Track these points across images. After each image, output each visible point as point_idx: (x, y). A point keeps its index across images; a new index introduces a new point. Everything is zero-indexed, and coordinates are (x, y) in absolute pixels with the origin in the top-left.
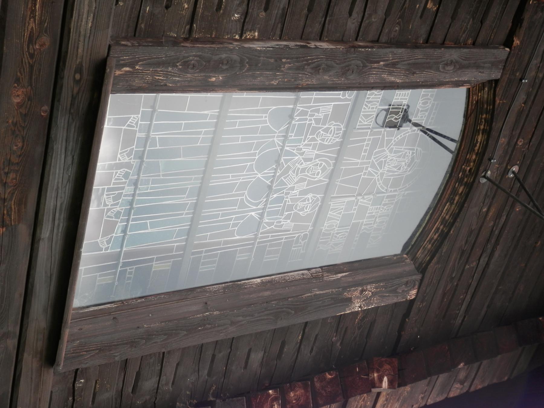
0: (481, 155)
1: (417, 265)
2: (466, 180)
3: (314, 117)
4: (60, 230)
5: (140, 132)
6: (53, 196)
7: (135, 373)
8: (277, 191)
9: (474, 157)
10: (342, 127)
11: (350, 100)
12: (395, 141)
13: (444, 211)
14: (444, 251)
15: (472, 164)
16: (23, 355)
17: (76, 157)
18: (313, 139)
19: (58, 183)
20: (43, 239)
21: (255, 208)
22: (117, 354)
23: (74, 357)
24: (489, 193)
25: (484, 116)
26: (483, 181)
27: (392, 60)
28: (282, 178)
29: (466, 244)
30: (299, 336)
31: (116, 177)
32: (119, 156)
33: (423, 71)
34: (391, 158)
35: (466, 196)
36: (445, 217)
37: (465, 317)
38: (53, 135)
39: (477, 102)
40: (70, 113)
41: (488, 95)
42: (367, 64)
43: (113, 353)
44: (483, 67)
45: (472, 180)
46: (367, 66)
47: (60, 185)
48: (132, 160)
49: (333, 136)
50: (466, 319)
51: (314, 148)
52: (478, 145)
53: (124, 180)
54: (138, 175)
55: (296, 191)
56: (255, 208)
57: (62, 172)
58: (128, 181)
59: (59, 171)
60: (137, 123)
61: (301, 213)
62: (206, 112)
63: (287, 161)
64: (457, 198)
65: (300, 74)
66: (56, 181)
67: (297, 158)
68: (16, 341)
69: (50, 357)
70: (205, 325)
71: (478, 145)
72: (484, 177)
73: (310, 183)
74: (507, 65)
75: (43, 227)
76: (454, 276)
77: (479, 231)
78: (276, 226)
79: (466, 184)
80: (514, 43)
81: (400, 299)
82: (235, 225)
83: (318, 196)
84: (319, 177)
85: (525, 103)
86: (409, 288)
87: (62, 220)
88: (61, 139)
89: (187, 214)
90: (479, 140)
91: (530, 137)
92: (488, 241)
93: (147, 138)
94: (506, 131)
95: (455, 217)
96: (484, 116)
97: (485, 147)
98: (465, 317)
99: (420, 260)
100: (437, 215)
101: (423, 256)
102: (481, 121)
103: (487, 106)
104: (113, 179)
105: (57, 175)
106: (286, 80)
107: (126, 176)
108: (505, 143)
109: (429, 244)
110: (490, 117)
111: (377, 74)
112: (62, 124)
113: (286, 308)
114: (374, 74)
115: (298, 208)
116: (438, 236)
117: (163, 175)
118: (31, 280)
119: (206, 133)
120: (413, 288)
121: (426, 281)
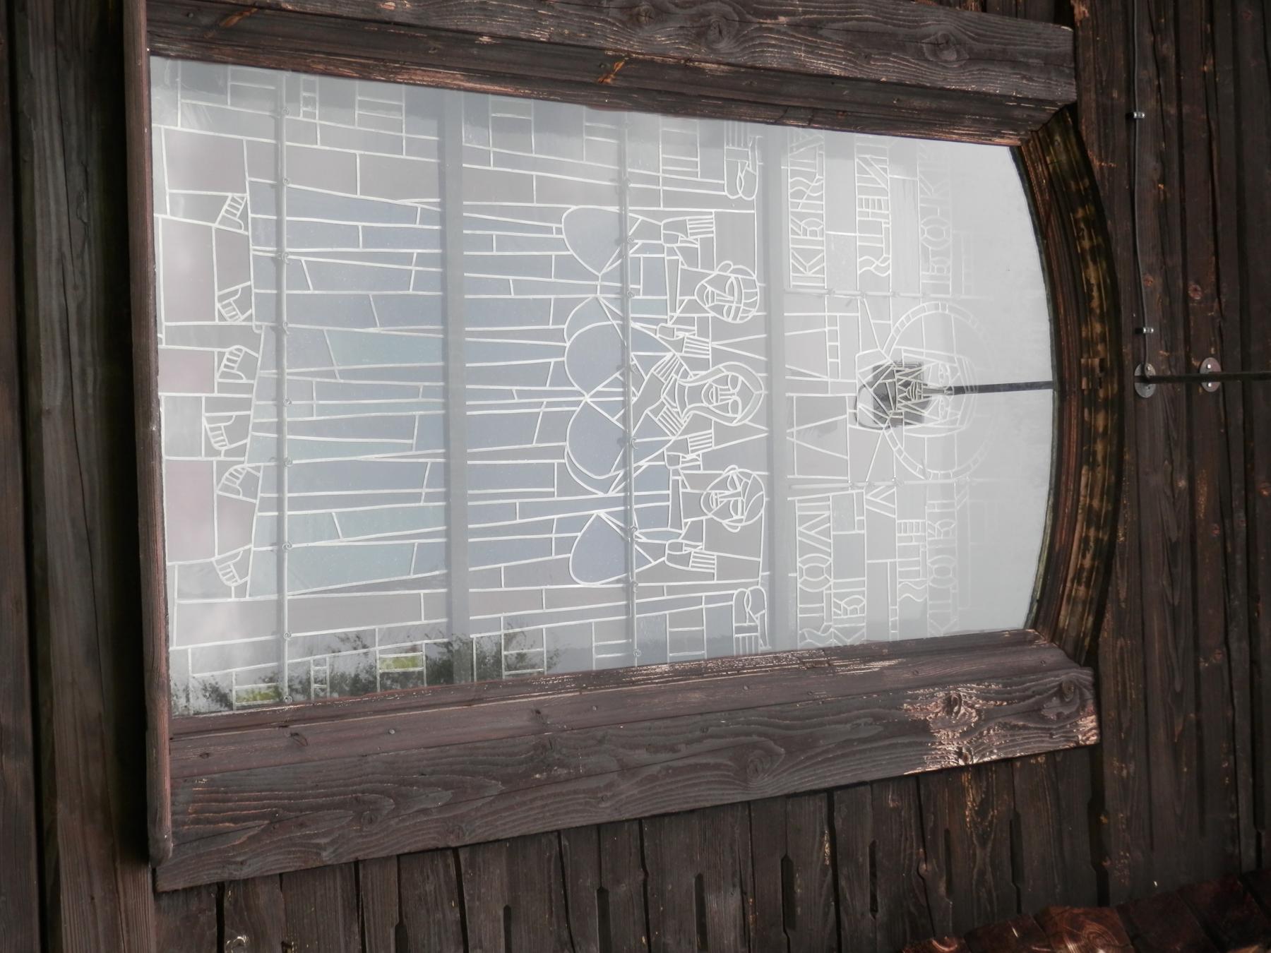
0: (1112, 314)
1: (1069, 648)
2: (1101, 393)
3: (679, 244)
4: (90, 390)
5: (257, 243)
6: (54, 281)
7: (392, 932)
8: (648, 449)
9: (1098, 328)
10: (755, 277)
11: (749, 205)
12: (897, 330)
13: (1083, 491)
14: (1123, 595)
15: (1100, 347)
16: (54, 813)
17: (94, 170)
18: (693, 306)
19: (60, 240)
20: (49, 412)
21: (601, 495)
22: (323, 841)
23: (201, 838)
24: (1174, 435)
25: (1080, 213)
26: (1148, 391)
27: (805, 13)
28: (647, 411)
29: (1172, 584)
30: (822, 845)
31: (222, 369)
32: (218, 305)
33: (889, 54)
34: (905, 379)
35: (1119, 435)
36: (1091, 506)
37: (1259, 837)
38: (24, 107)
39: (1050, 181)
40: (56, 42)
41: (1067, 151)
42: (749, 17)
43: (310, 837)
44: (1027, 66)
45: (1116, 386)
46: (750, 22)
47: (66, 249)
48: (254, 323)
49: (740, 301)
50: (1264, 844)
51: (703, 332)
52: (1095, 293)
53: (244, 381)
54: (279, 366)
55: (693, 456)
56: (601, 495)
57: (64, 208)
58: (255, 382)
59: (57, 202)
60: (244, 216)
61: (725, 522)
62: (408, 202)
63: (648, 363)
64: (1099, 447)
65: (595, 19)
66: (54, 236)
67: (668, 355)
68: (26, 764)
69: (131, 834)
70: (549, 767)
71: (1095, 293)
72: (1145, 380)
73: (723, 433)
74: (1081, 65)
75: (43, 374)
76: (1178, 688)
77: (1193, 542)
78: (671, 558)
79: (1107, 404)
80: (1076, 11)
81: (1059, 743)
82: (564, 545)
83: (755, 474)
84: (739, 416)
85: (1163, 180)
86: (1074, 709)
87: (89, 358)
88: (45, 111)
89: (430, 497)
90: (1093, 281)
91: (1213, 278)
92: (1228, 584)
93: (277, 262)
94: (1147, 257)
95: (1114, 493)
96: (1080, 213)
97: (1112, 291)
98: (1259, 837)
99: (1073, 634)
100: (1069, 503)
101: (1075, 620)
102: (1079, 230)
103: (1077, 184)
104: (217, 375)
105: (53, 219)
106: (566, 32)
107: (248, 366)
108: (1159, 289)
109: (1079, 584)
110: (1093, 209)
111: (781, 47)
112: (43, 71)
113: (760, 735)
114: (773, 46)
115: (715, 508)
116: (1093, 559)
117: (344, 374)
118: (37, 552)
119: (423, 260)
120: (1080, 711)
121: (1109, 686)
